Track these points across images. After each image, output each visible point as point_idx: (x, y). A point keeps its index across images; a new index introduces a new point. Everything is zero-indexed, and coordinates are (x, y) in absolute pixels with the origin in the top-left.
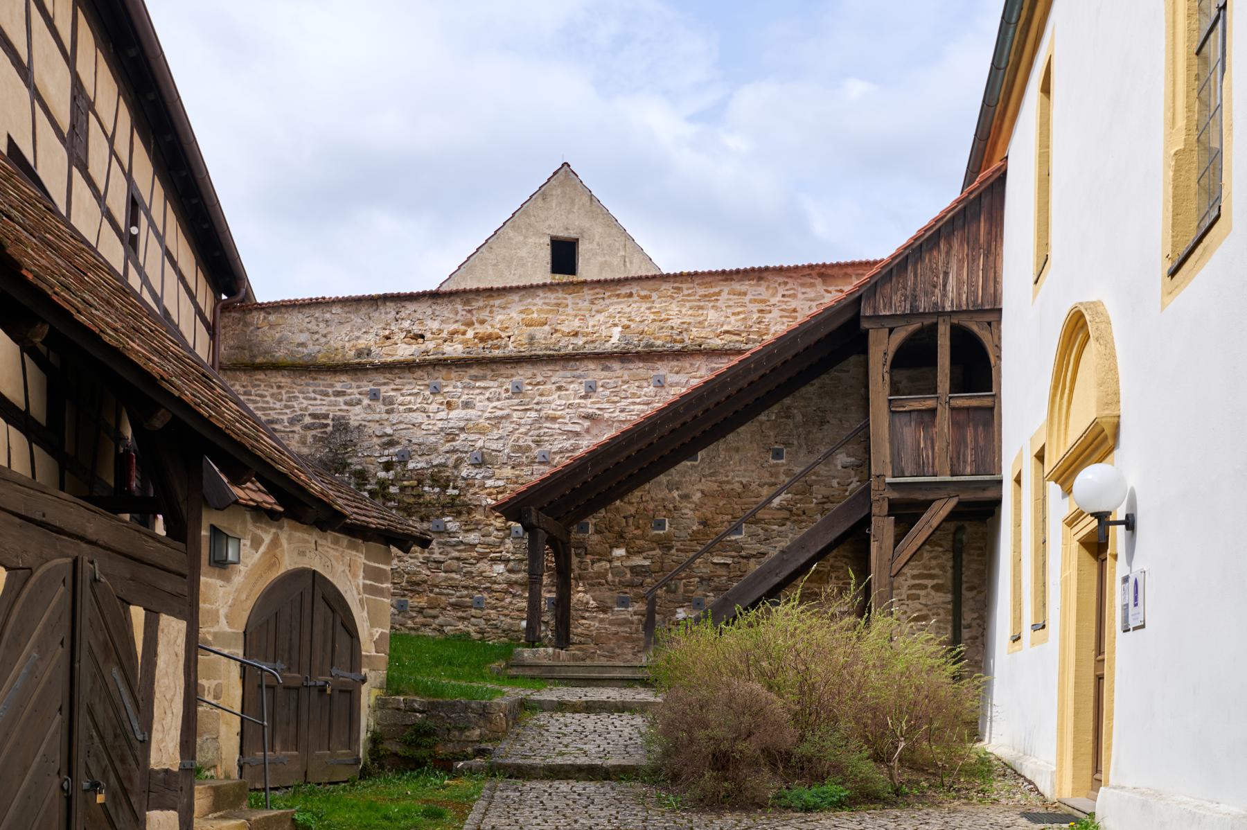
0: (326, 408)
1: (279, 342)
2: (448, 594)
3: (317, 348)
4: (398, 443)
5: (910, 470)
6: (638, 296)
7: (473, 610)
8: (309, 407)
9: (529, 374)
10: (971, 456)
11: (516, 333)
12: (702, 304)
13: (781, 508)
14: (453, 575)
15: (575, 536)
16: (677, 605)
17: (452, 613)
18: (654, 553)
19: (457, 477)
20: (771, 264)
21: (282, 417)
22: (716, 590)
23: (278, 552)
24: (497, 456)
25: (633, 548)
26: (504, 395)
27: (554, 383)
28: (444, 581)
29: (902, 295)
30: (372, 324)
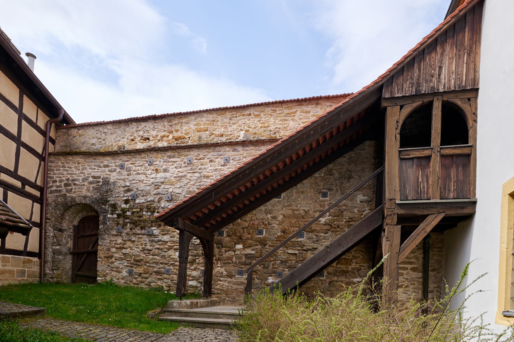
0: (100, 173)
1: (83, 143)
2: (153, 267)
3: (100, 146)
4: (132, 190)
5: (411, 196)
6: (254, 115)
7: (165, 275)
8: (92, 173)
9: (196, 154)
10: (454, 186)
11: (192, 136)
12: (286, 118)
13: (326, 224)
14: (156, 257)
15: (216, 237)
16: (268, 275)
17: (155, 276)
18: (257, 247)
19: (159, 207)
20: (323, 95)
21: (79, 178)
22: (290, 267)
24: (179, 196)
25: (246, 244)
26: (183, 165)
27: (208, 159)
28: (151, 260)
29: (410, 83)
30: (126, 134)
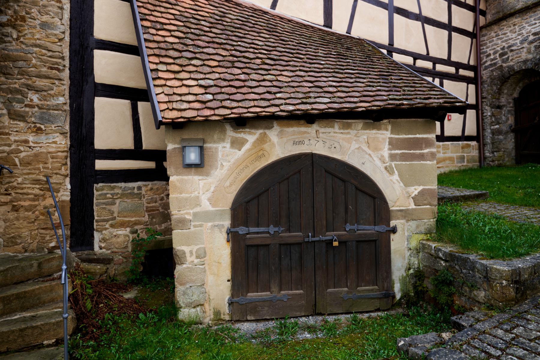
8: (532, 30)
23: (266, 146)
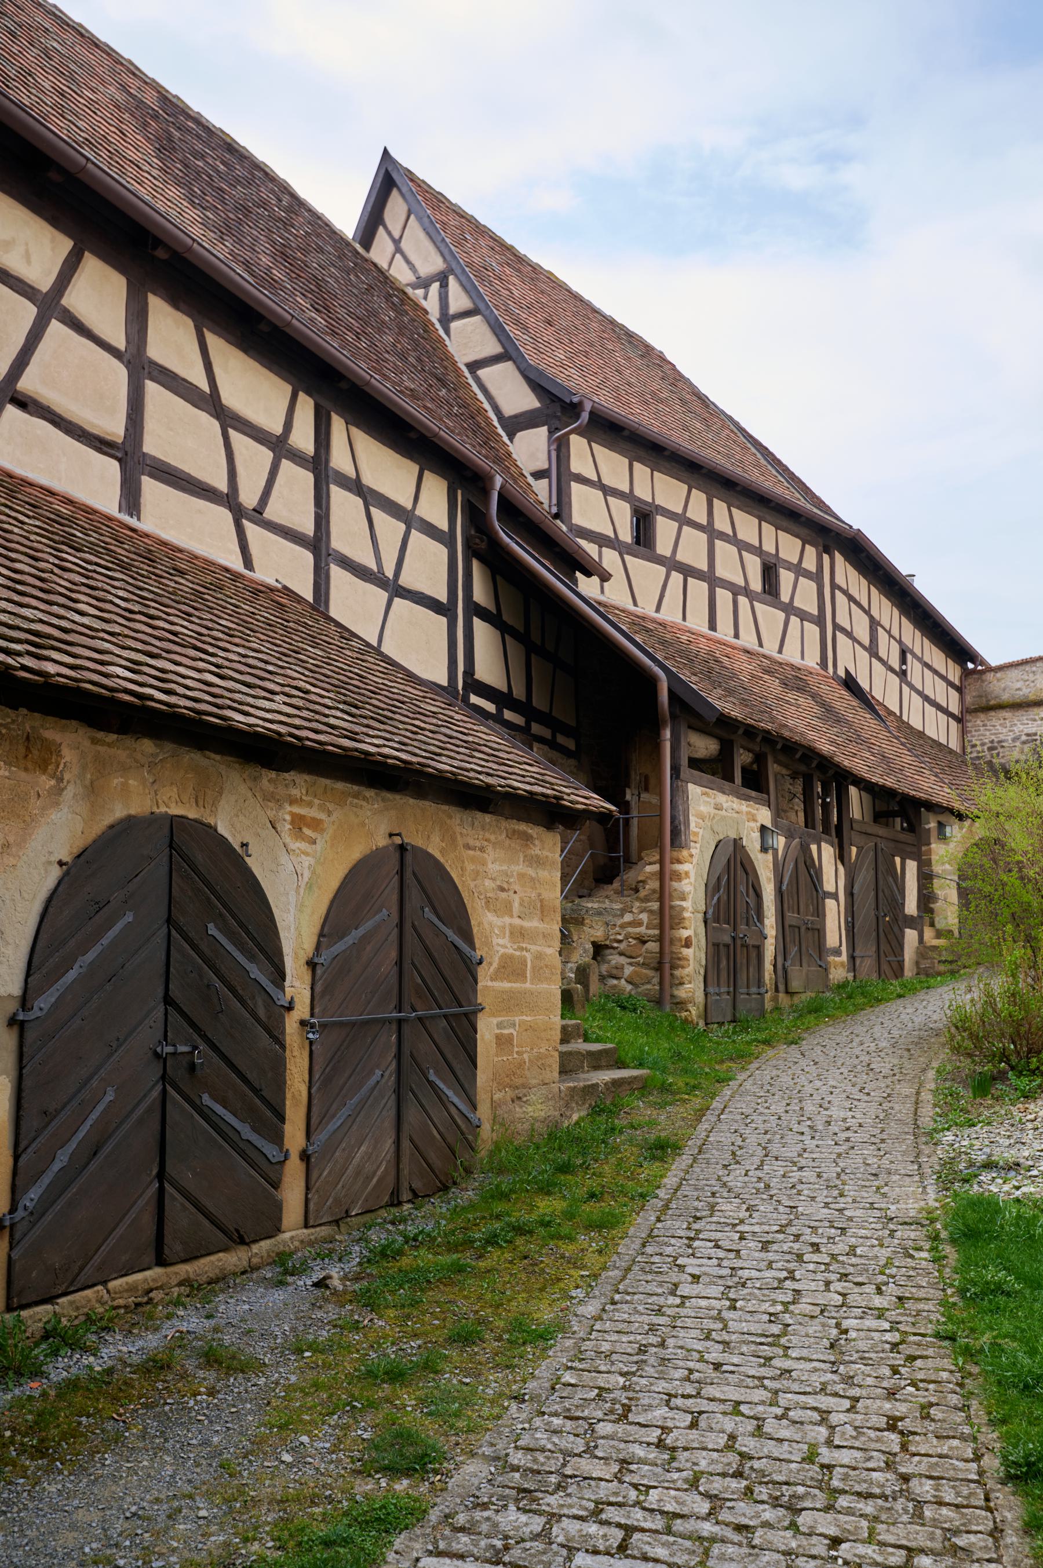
1: (1004, 690)
